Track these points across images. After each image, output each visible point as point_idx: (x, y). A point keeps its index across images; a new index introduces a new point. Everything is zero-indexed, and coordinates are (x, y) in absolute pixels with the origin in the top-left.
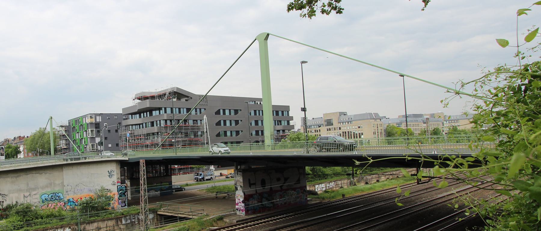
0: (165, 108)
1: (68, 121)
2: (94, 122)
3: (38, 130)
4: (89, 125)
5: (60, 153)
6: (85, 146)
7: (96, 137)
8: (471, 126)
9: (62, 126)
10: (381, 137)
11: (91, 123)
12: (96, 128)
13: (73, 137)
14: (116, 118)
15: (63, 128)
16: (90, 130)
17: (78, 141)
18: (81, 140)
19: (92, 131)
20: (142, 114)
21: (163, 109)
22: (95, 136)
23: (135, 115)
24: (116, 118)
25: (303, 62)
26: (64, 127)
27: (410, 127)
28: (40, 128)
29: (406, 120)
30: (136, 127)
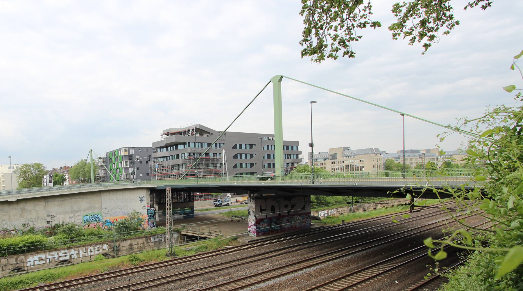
4: (124, 157)
6: (120, 175)
7: (129, 167)
9: (100, 158)
12: (130, 159)
13: (110, 167)
16: (124, 161)
18: (117, 170)
19: (126, 162)
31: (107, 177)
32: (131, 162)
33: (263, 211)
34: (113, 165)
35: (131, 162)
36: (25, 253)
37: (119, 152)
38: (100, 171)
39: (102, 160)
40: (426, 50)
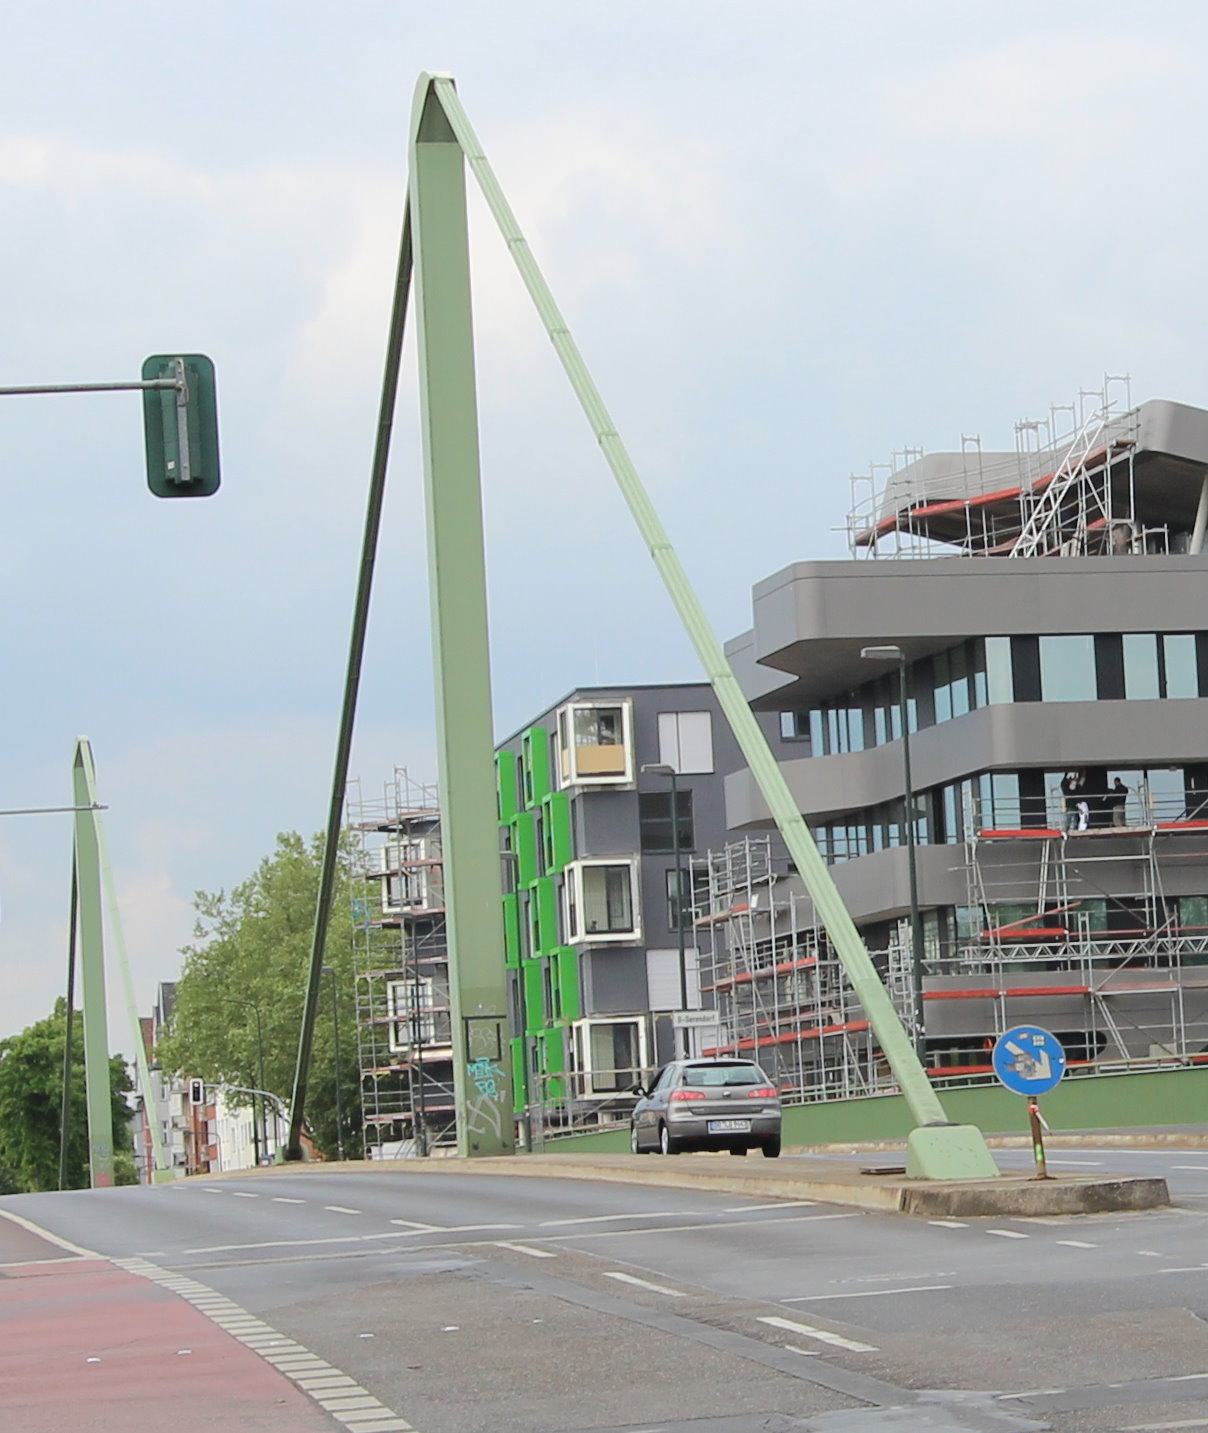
0: (1025, 649)
2: (629, 778)
7: (653, 941)
8: (128, 1059)
10: (450, 1047)
11: (599, 797)
12: (651, 842)
20: (938, 692)
21: (999, 656)
22: (637, 934)
23: (842, 712)
25: (453, 82)
30: (852, 835)
38: (403, 988)
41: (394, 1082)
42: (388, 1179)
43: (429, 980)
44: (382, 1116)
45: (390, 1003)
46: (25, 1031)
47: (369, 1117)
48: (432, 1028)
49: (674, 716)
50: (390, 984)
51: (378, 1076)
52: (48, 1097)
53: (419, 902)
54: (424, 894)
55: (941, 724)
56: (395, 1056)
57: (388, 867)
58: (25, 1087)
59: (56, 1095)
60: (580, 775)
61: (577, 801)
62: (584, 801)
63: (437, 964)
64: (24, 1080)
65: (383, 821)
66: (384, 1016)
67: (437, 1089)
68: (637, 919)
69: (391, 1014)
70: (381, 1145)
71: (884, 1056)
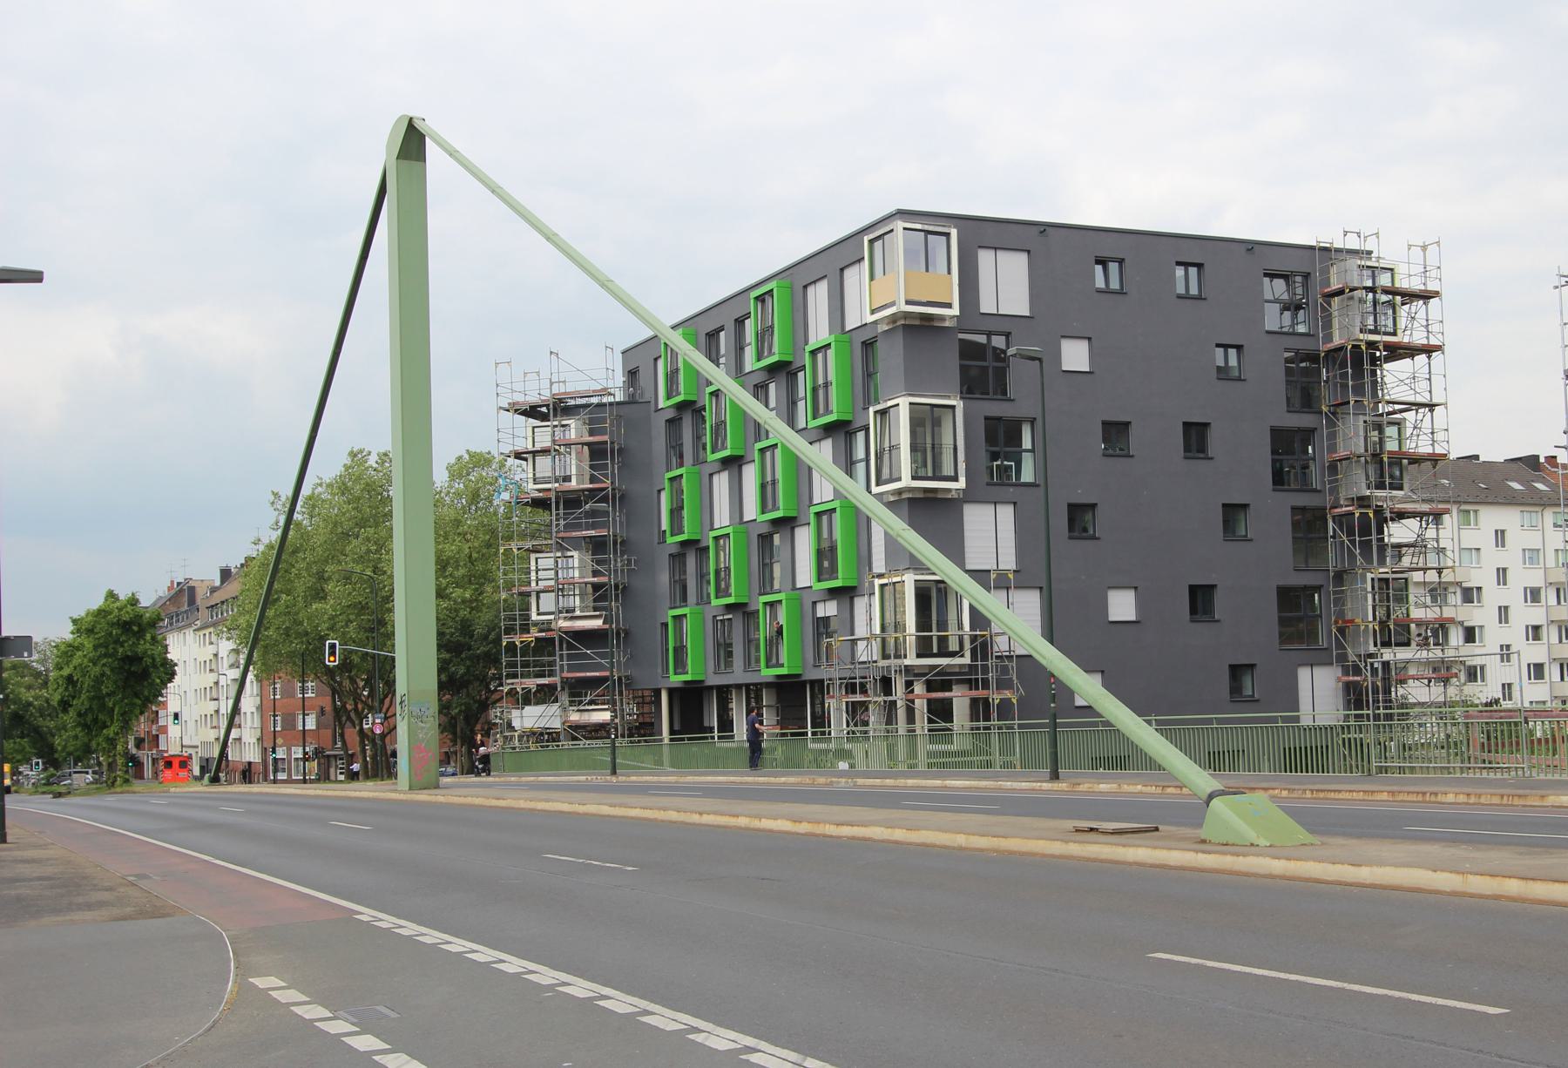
1: (619, 358)
2: (955, 311)
3: (97, 602)
4: (891, 357)
5: (532, 683)
6: (829, 609)
7: (969, 496)
9: (560, 408)
12: (972, 386)
13: (676, 512)
14: (1115, 285)
15: (571, 422)
16: (903, 406)
17: (734, 559)
18: (765, 540)
19: (926, 422)
22: (962, 483)
24: (1115, 284)
26: (584, 415)
27: (930, 754)
28: (111, 595)
29: (614, 753)
31: (625, 636)
32: (992, 423)
33: (780, 662)
34: (722, 482)
35: (992, 423)
36: (358, 779)
37: (819, 296)
38: (547, 561)
39: (574, 429)
40: (1441, 299)
41: (545, 645)
42: (187, 795)
43: (575, 554)
44: (523, 680)
45: (533, 574)
46: (169, 589)
47: (509, 681)
48: (577, 598)
49: (993, 252)
50: (533, 556)
51: (522, 642)
52: (142, 658)
53: (567, 479)
54: (574, 472)
55: (1262, 284)
56: (536, 624)
57: (534, 446)
58: (121, 650)
59: (148, 656)
60: (908, 303)
61: (880, 347)
62: (904, 335)
63: (584, 538)
64: (117, 642)
65: (533, 399)
66: (527, 586)
67: (586, 656)
68: (962, 466)
69: (533, 584)
70: (523, 708)
71: (258, 782)
